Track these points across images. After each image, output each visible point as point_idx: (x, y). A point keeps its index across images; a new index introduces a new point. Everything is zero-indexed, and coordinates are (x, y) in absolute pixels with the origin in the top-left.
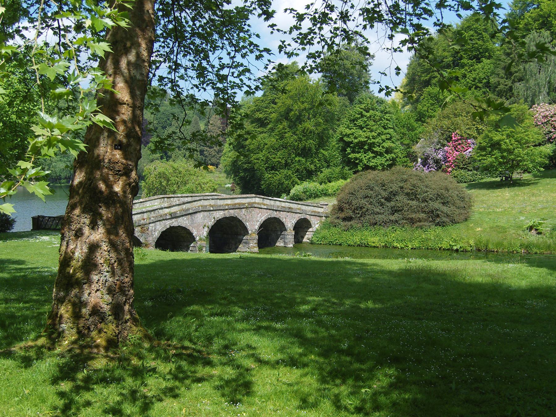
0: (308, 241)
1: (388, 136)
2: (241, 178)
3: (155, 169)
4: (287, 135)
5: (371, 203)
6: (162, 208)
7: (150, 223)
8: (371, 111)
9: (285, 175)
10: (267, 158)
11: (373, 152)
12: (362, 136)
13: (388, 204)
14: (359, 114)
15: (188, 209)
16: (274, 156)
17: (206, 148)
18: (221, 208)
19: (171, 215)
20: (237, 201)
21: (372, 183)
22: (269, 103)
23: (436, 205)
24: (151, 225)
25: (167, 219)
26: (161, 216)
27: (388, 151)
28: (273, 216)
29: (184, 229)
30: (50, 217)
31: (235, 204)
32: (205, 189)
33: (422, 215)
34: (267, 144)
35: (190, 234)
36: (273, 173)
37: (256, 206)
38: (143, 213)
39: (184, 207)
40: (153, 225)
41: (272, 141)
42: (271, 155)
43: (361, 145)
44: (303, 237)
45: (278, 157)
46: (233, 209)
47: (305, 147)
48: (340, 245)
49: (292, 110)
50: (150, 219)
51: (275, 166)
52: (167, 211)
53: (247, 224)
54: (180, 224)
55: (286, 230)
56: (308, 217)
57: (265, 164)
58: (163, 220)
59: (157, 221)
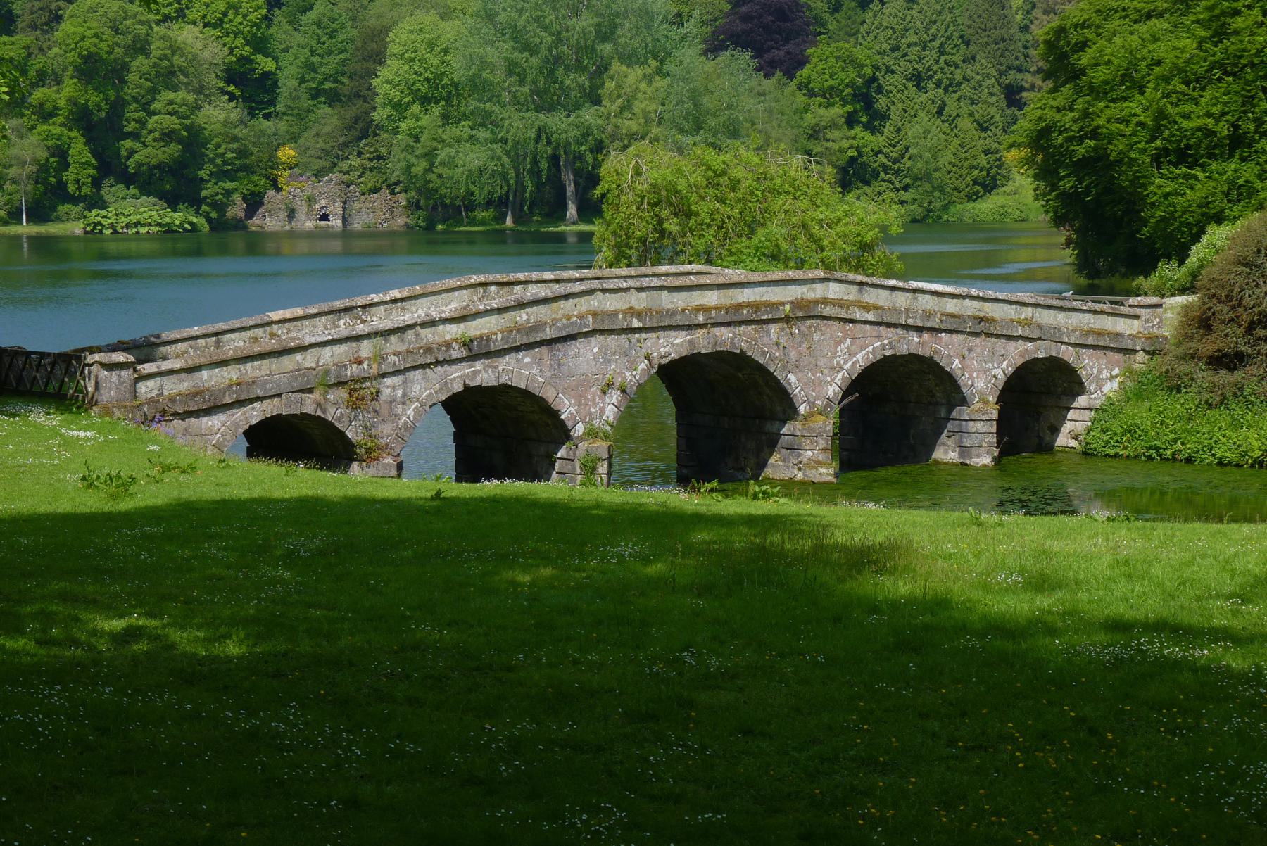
0: (1074, 443)
2: (1065, 197)
3: (638, 173)
4: (1239, 22)
6: (431, 323)
7: (383, 375)
9: (1228, 181)
10: (1161, 115)
15: (540, 326)
16: (1186, 108)
17: (1029, 77)
18: (678, 320)
19: (467, 344)
20: (747, 295)
24: (387, 381)
25: (451, 362)
26: (428, 350)
28: (904, 349)
29: (525, 394)
30: (43, 355)
31: (739, 307)
32: (825, 242)
34: (1159, 63)
35: (552, 414)
36: (1185, 177)
37: (827, 311)
38: (358, 338)
39: (522, 316)
40: (396, 380)
42: (1175, 105)
44: (1055, 430)
45: (1202, 113)
46: (729, 324)
48: (1189, 460)
50: (384, 359)
51: (1188, 147)
52: (451, 331)
53: (792, 381)
54: (504, 379)
55: (964, 401)
57: (1153, 139)
58: (437, 363)
59: (415, 368)
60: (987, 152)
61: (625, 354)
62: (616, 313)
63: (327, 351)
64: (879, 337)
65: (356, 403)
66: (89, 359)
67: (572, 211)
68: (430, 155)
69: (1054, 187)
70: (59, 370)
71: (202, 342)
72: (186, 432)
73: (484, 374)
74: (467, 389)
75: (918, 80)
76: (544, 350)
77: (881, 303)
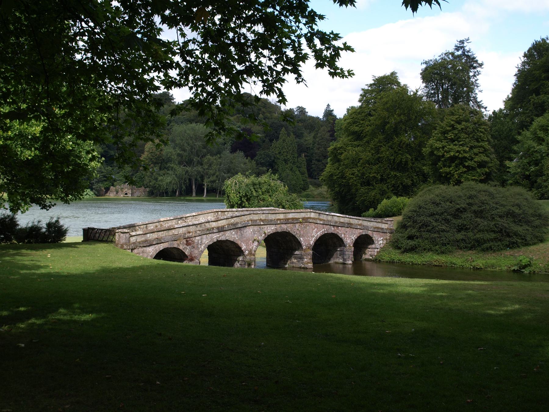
0: (371, 258)
1: (481, 150)
4: (382, 149)
5: (436, 221)
7: (195, 237)
8: (464, 123)
11: (464, 166)
12: (454, 149)
13: (454, 221)
14: (450, 126)
15: (237, 223)
18: (273, 222)
19: (218, 228)
21: (437, 200)
22: (366, 116)
23: (505, 223)
24: (197, 238)
26: (208, 230)
27: (482, 165)
28: (330, 231)
29: (233, 243)
33: (493, 235)
35: (240, 248)
37: (311, 221)
39: (232, 221)
41: (366, 155)
43: (453, 159)
47: (401, 161)
49: (388, 123)
54: (227, 238)
55: (345, 246)
56: (370, 233)
60: (303, 180)
61: (259, 232)
62: (257, 220)
63: (181, 230)
64: (324, 228)
65: (188, 244)
66: (117, 231)
67: (194, 194)
68: (156, 179)
69: (332, 190)
70: (108, 233)
71: (142, 226)
72: (143, 252)
73: (222, 237)
74: (218, 241)
75: (286, 161)
76: (238, 230)
77: (324, 219)
